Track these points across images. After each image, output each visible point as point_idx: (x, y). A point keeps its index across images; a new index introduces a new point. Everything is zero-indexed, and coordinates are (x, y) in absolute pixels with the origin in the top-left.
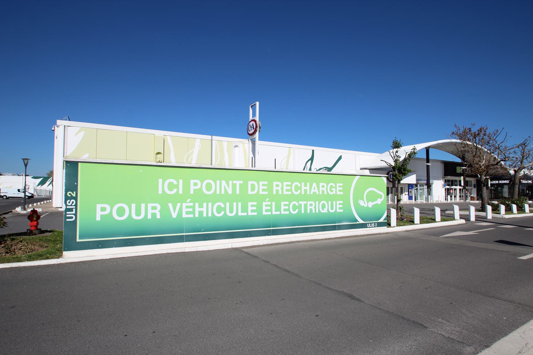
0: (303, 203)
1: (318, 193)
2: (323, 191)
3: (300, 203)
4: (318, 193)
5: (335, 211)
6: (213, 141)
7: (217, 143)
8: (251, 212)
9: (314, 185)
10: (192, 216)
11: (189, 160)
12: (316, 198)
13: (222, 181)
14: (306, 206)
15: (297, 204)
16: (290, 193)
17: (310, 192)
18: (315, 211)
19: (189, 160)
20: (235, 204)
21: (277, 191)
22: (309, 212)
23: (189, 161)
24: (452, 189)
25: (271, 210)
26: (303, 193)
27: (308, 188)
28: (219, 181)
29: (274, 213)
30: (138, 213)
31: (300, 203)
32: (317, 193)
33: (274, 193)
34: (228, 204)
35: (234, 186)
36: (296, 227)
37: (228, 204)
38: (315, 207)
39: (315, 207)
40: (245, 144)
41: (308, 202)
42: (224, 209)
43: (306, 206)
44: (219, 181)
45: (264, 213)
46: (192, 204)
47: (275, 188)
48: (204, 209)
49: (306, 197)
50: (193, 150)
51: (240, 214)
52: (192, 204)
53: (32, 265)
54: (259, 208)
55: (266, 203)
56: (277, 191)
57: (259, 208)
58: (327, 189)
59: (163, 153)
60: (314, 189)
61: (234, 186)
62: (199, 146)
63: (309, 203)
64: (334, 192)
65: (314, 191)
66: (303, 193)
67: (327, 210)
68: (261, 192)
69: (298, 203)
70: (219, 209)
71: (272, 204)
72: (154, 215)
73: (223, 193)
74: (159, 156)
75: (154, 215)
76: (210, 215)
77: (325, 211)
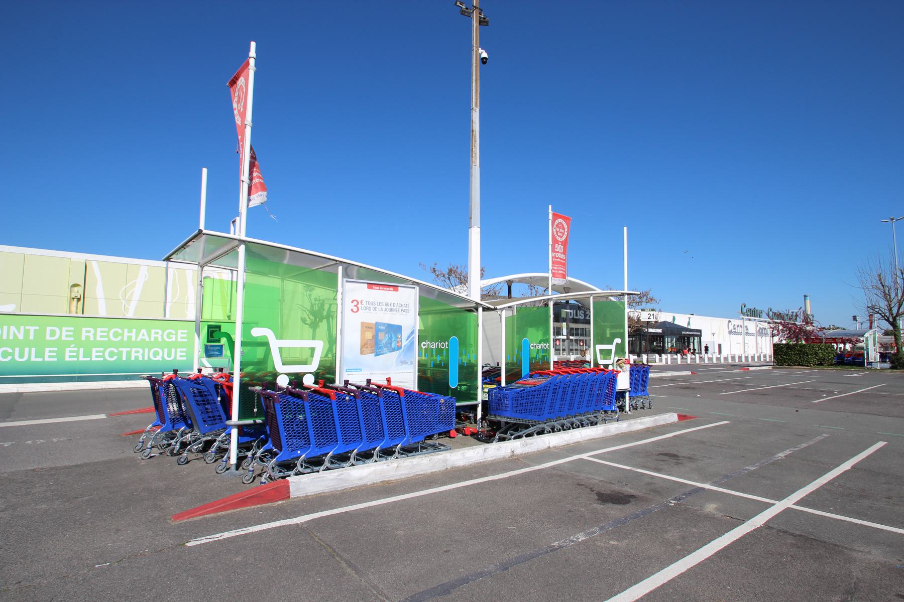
0: (125, 350)
1: (149, 340)
2: (156, 338)
3: (120, 349)
4: (149, 340)
5: (173, 359)
6: (169, 269)
7: (176, 271)
8: (49, 356)
9: (144, 331)
10: (76, 359)
11: (128, 295)
12: (144, 344)
13: (11, 327)
14: (129, 353)
15: (116, 351)
16: (106, 339)
17: (136, 338)
18: (143, 358)
19: (128, 295)
20: (27, 349)
21: (88, 337)
22: (133, 359)
23: (127, 297)
24: (559, 340)
25: (77, 356)
26: (125, 339)
27: (133, 334)
28: (6, 327)
29: (81, 359)
30: (169, 355)
31: (120, 349)
32: (147, 339)
33: (83, 339)
34: (17, 350)
35: (27, 332)
36: (114, 374)
37: (17, 350)
38: (143, 355)
39: (143, 355)
40: (223, 274)
41: (133, 349)
42: (13, 354)
43: (129, 353)
44: (6, 327)
45: (67, 359)
46: (76, 349)
47: (84, 335)
48: (140, 355)
49: (130, 344)
50: (135, 281)
51: (33, 359)
52: (76, 349)
53: (743, 496)
54: (61, 354)
55: (71, 349)
56: (88, 337)
57: (61, 354)
58: (162, 336)
59: (230, 321)
60: (143, 335)
61: (27, 332)
62: (146, 275)
63: (134, 350)
64: (174, 339)
65: (143, 337)
66: (125, 339)
67: (162, 358)
68: (64, 338)
69: (118, 350)
70: (111, 354)
71: (79, 349)
72: (137, 357)
73: (11, 337)
74: (76, 289)
75: (137, 357)
76: (146, 359)
77: (159, 358)
